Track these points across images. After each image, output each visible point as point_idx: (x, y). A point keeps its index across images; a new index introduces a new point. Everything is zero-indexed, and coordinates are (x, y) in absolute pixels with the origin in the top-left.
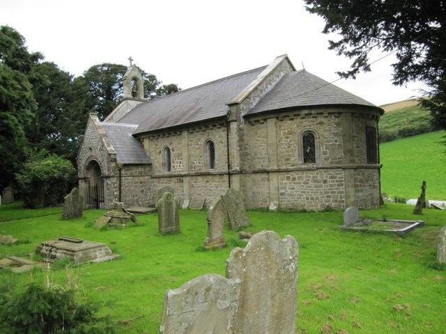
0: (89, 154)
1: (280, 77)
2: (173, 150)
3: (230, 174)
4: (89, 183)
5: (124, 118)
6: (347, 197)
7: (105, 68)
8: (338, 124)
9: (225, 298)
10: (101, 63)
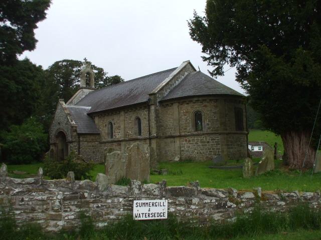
0: (58, 127)
1: (185, 76)
2: (114, 124)
3: (150, 139)
4: (58, 147)
5: (79, 103)
6: (223, 151)
7: (64, 64)
8: (216, 107)
9: (123, 159)
10: (61, 59)
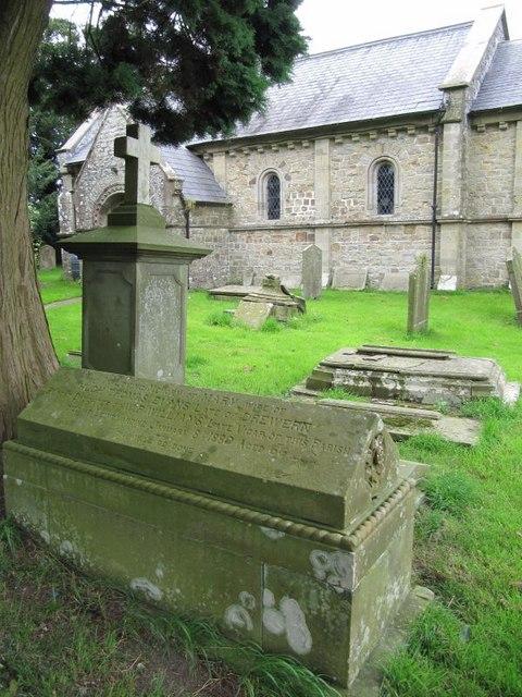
2: (288, 178)
3: (435, 224)
